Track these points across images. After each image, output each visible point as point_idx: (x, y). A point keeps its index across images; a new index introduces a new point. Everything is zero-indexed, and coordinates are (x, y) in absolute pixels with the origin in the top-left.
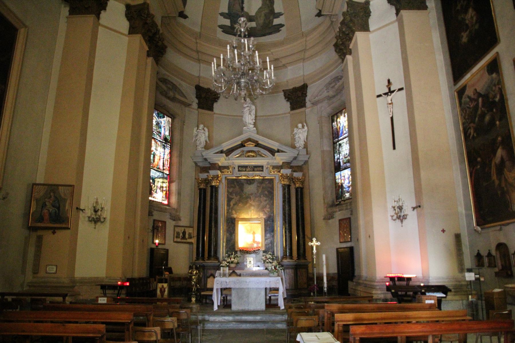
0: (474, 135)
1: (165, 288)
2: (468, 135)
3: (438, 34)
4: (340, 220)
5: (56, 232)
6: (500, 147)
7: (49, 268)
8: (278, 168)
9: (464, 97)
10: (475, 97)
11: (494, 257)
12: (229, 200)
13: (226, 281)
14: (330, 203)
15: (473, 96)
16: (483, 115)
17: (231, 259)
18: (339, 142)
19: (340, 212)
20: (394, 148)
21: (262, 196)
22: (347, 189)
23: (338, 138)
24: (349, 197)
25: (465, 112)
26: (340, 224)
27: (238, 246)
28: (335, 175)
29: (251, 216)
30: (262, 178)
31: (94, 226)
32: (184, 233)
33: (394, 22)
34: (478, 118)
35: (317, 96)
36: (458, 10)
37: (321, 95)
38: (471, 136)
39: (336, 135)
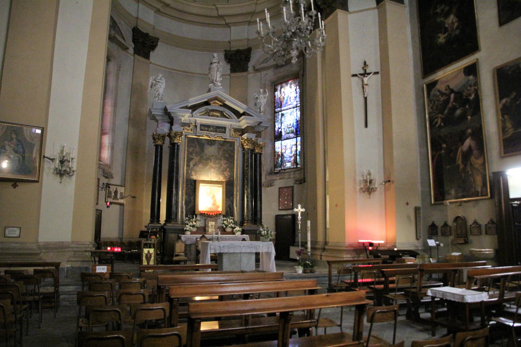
1: (151, 254)
2: (434, 123)
3: (410, 29)
4: (280, 188)
5: (17, 186)
6: (469, 138)
7: (8, 231)
8: (242, 131)
9: (434, 90)
10: (447, 92)
11: (450, 227)
12: (189, 160)
13: (240, 245)
14: (269, 171)
15: (444, 91)
16: (454, 109)
17: (192, 222)
18: (282, 112)
19: (280, 181)
20: (366, 126)
21: (223, 158)
22: (288, 159)
23: (281, 108)
24: (290, 167)
25: (433, 103)
26: (279, 192)
27: (198, 209)
28: (275, 143)
29: (211, 179)
30: (224, 140)
31: (60, 181)
32: (116, 192)
33: (374, 8)
35: (262, 63)
36: (437, 13)
38: (437, 125)
39: (278, 105)
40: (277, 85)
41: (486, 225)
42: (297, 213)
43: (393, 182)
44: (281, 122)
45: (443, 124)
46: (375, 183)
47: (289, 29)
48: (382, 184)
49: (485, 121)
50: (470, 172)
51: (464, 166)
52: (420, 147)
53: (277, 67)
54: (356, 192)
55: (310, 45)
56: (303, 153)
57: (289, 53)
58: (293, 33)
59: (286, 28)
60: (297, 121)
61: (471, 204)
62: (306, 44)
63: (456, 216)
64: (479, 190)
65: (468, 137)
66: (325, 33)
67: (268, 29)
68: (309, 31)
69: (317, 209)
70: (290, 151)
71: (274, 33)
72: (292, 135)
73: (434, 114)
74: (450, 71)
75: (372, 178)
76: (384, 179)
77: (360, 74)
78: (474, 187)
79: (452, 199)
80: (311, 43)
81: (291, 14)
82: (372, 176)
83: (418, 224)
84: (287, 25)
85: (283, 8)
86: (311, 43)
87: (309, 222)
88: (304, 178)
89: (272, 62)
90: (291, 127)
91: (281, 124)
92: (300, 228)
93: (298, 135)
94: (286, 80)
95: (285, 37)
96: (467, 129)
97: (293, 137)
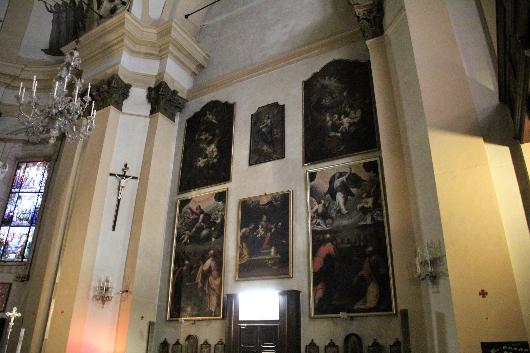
0: (187, 241)
2: (181, 238)
6: (211, 258)
9: (186, 207)
11: (182, 345)
15: (195, 210)
16: (201, 229)
18: (20, 194)
20: (114, 229)
22: (14, 249)
23: (20, 189)
24: (13, 259)
34: (195, 229)
35: (11, 133)
36: (201, 139)
37: (16, 134)
38: (184, 241)
39: (17, 184)
40: (22, 162)
41: (215, 345)
42: (10, 318)
43: (131, 293)
44: (16, 205)
45: (190, 241)
46: (112, 290)
47: (56, 106)
48: (118, 293)
49: (226, 245)
50: (207, 292)
51: (202, 285)
52: (164, 259)
53: (27, 142)
54: (88, 299)
55: (74, 130)
56: (34, 246)
57: (48, 131)
58: (59, 111)
59: (53, 104)
60: (36, 208)
61: (204, 323)
62: (70, 127)
63: (188, 335)
64: (213, 310)
65: (209, 258)
66: (94, 123)
67: (32, 98)
68: (78, 115)
69: (36, 315)
70: (18, 240)
71: (36, 104)
72: (25, 223)
73: (183, 230)
74: (203, 193)
75: (109, 286)
76: (123, 288)
77: (118, 175)
78: (209, 307)
79: (187, 317)
80: (76, 128)
81: (64, 92)
82: (110, 283)
83: (149, 341)
84: (55, 101)
85: (55, 83)
86: (76, 127)
87: (23, 331)
88: (28, 276)
89: (23, 136)
90: (27, 213)
91: (15, 208)
92: (8, 338)
93: (33, 225)
94: (34, 160)
95: (49, 113)
96: (210, 250)
97: (26, 225)
